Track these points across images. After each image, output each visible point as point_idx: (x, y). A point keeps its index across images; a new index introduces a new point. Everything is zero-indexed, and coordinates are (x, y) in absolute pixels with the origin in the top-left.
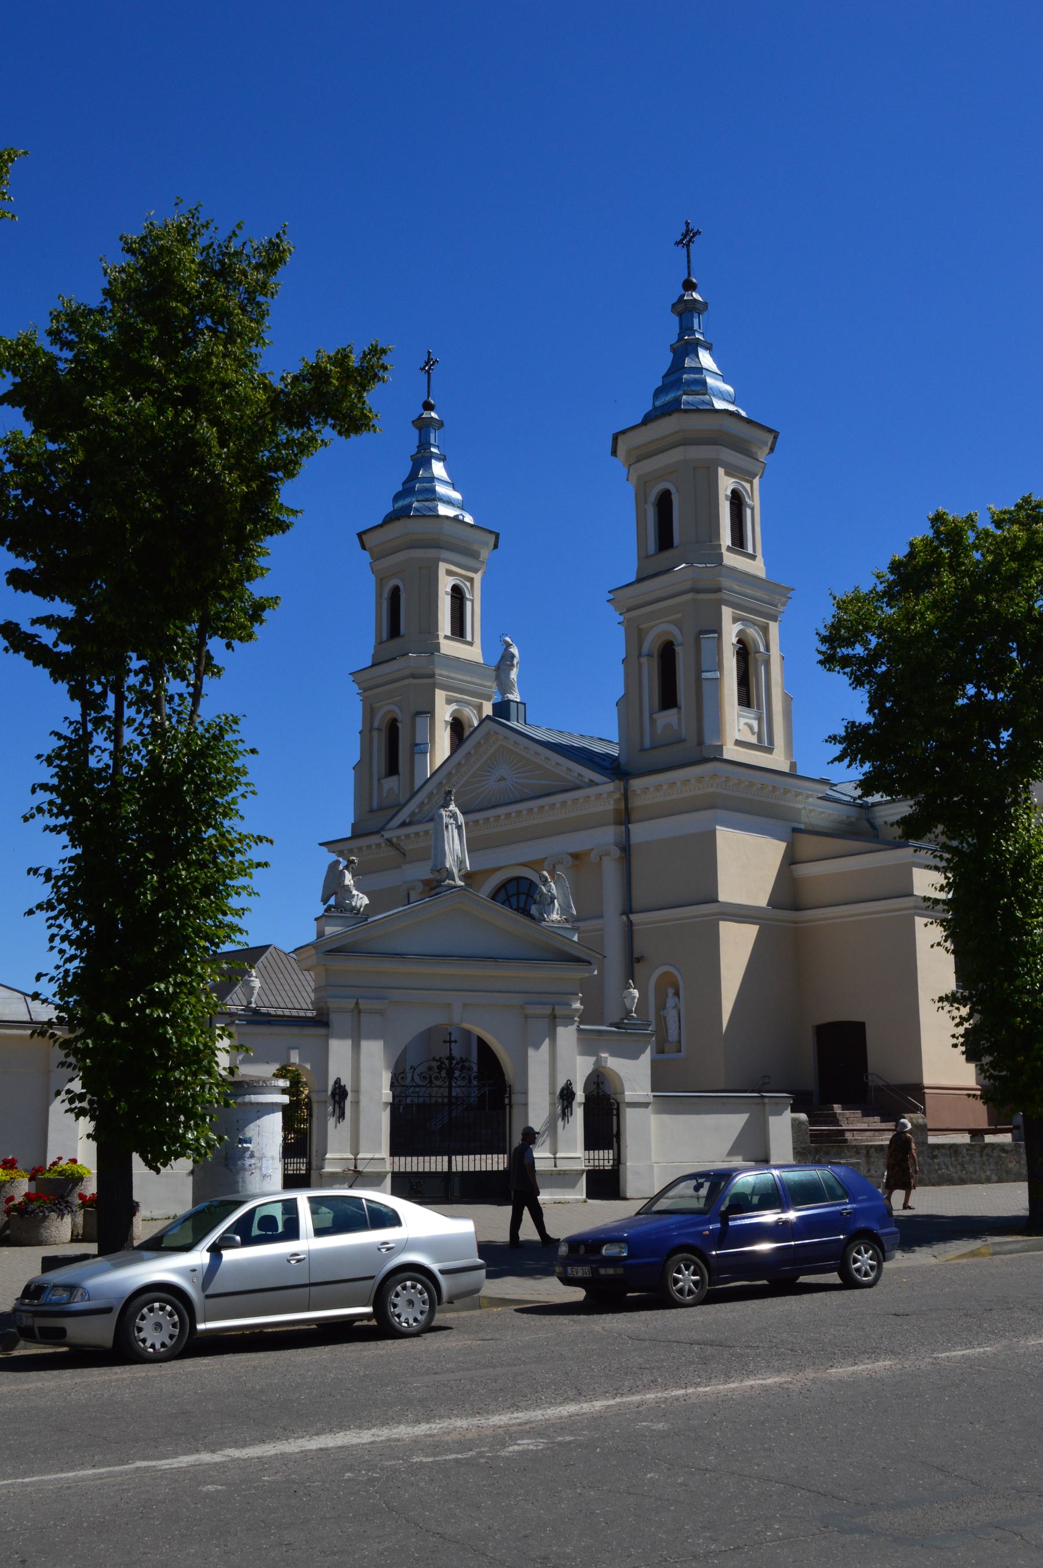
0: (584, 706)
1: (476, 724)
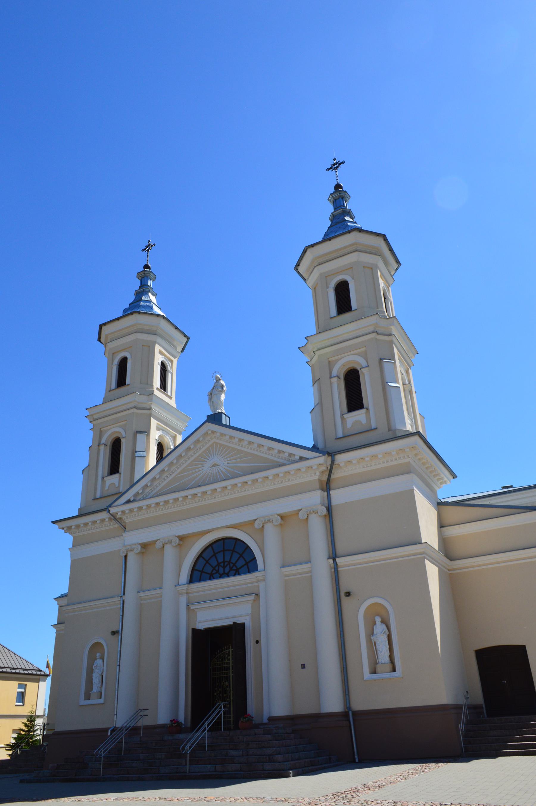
0: (288, 408)
1: (172, 447)
